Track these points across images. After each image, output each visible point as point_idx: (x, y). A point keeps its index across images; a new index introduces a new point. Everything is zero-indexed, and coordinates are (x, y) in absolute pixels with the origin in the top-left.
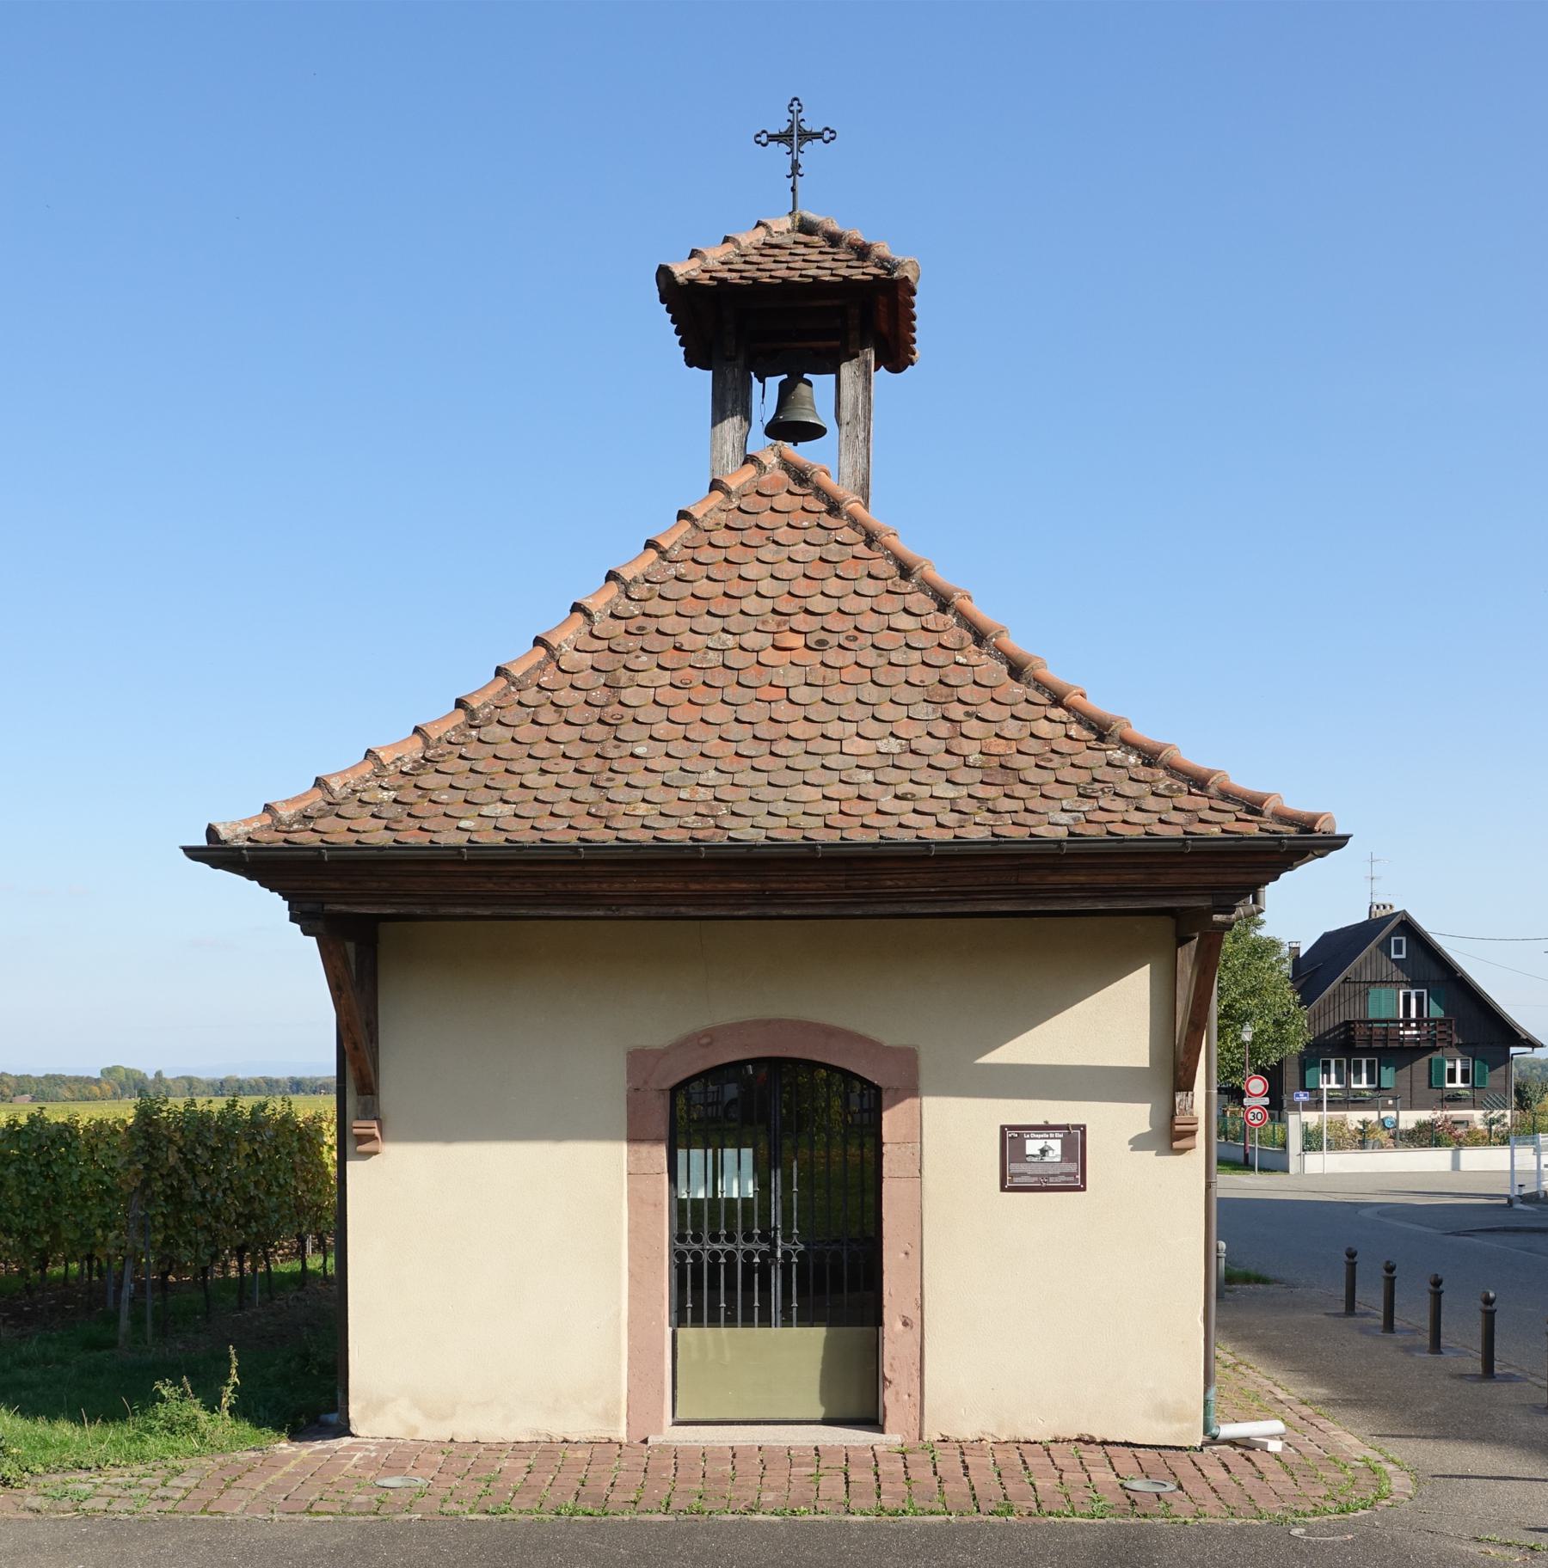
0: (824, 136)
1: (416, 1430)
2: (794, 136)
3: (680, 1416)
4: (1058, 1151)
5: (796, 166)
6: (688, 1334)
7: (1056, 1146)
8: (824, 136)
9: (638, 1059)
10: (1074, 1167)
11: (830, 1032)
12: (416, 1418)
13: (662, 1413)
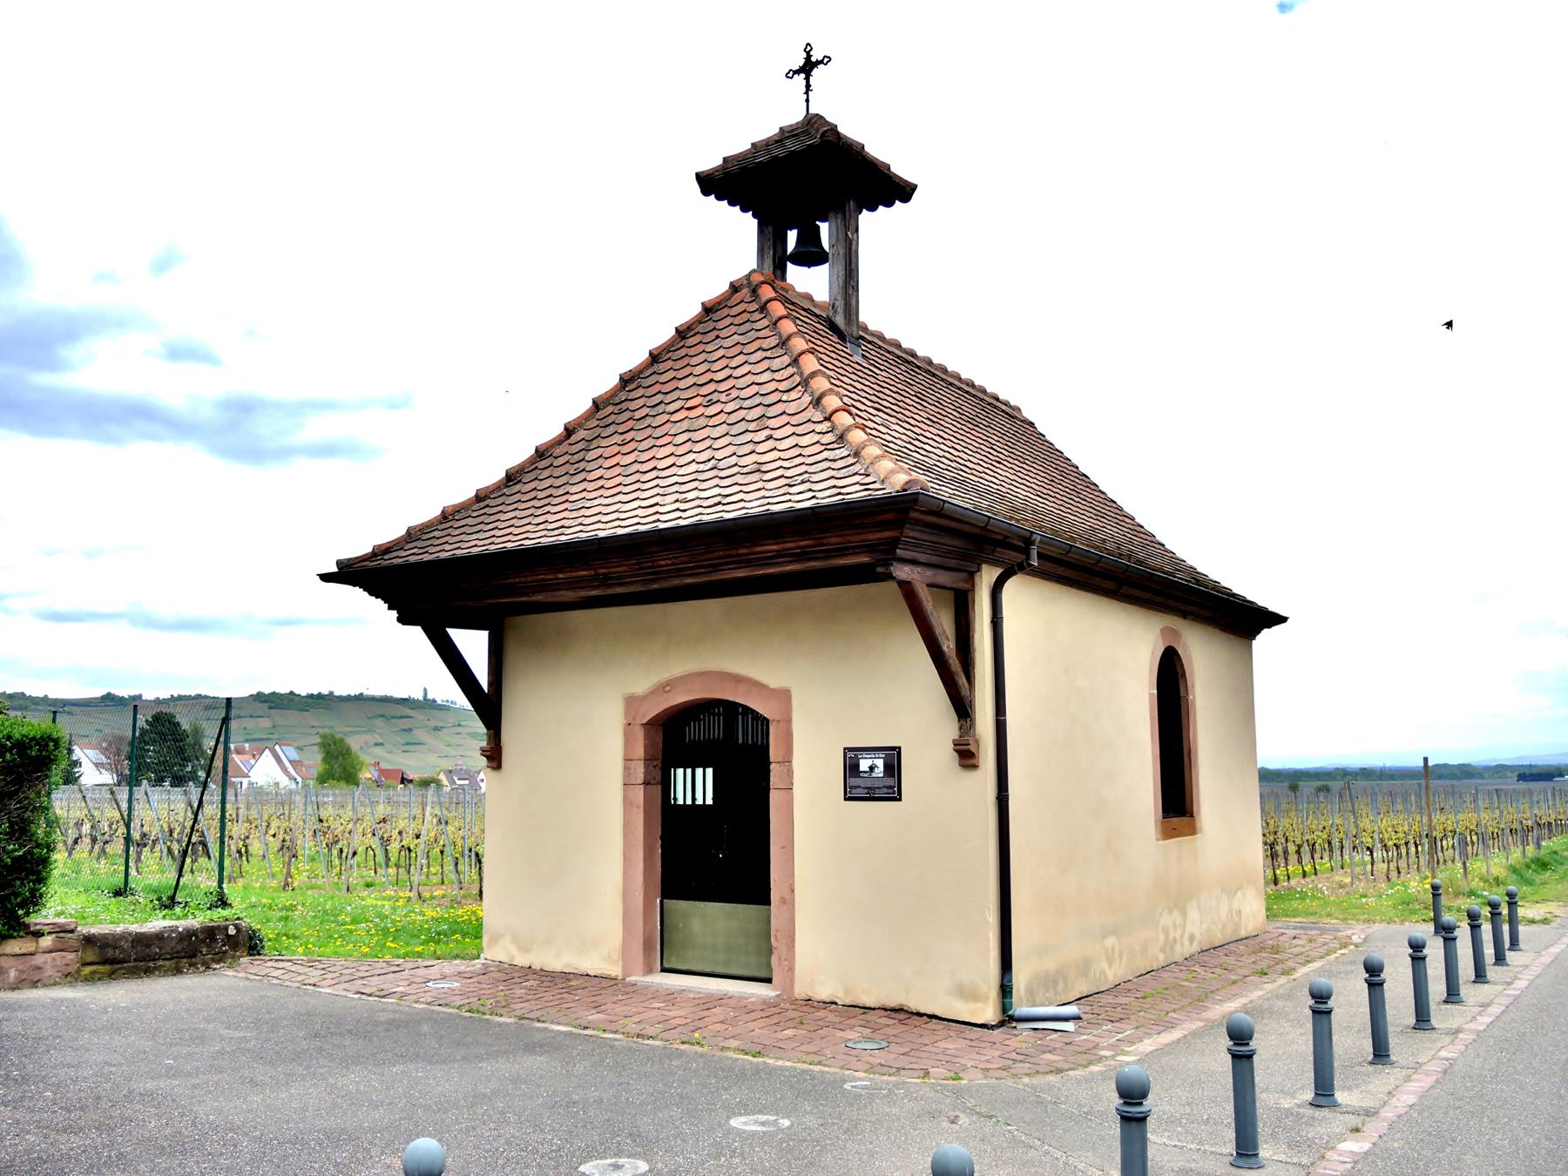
0: (825, 61)
1: (513, 958)
2: (808, 67)
3: (666, 965)
4: (881, 768)
5: (808, 86)
6: (679, 906)
7: (880, 763)
8: (825, 61)
9: (631, 702)
10: (890, 781)
11: (738, 680)
12: (513, 949)
13: (62, 1000)
